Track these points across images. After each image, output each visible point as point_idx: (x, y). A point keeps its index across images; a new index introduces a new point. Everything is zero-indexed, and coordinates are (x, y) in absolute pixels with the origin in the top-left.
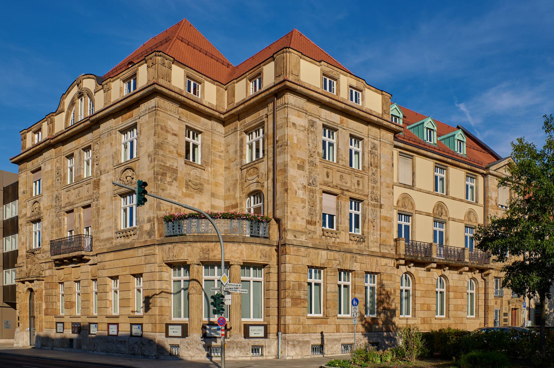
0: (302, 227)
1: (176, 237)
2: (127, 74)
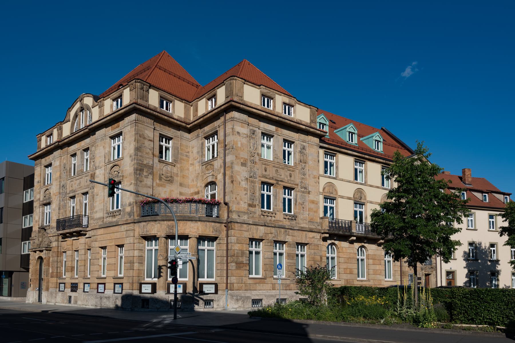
1: (149, 217)
2: (115, 95)
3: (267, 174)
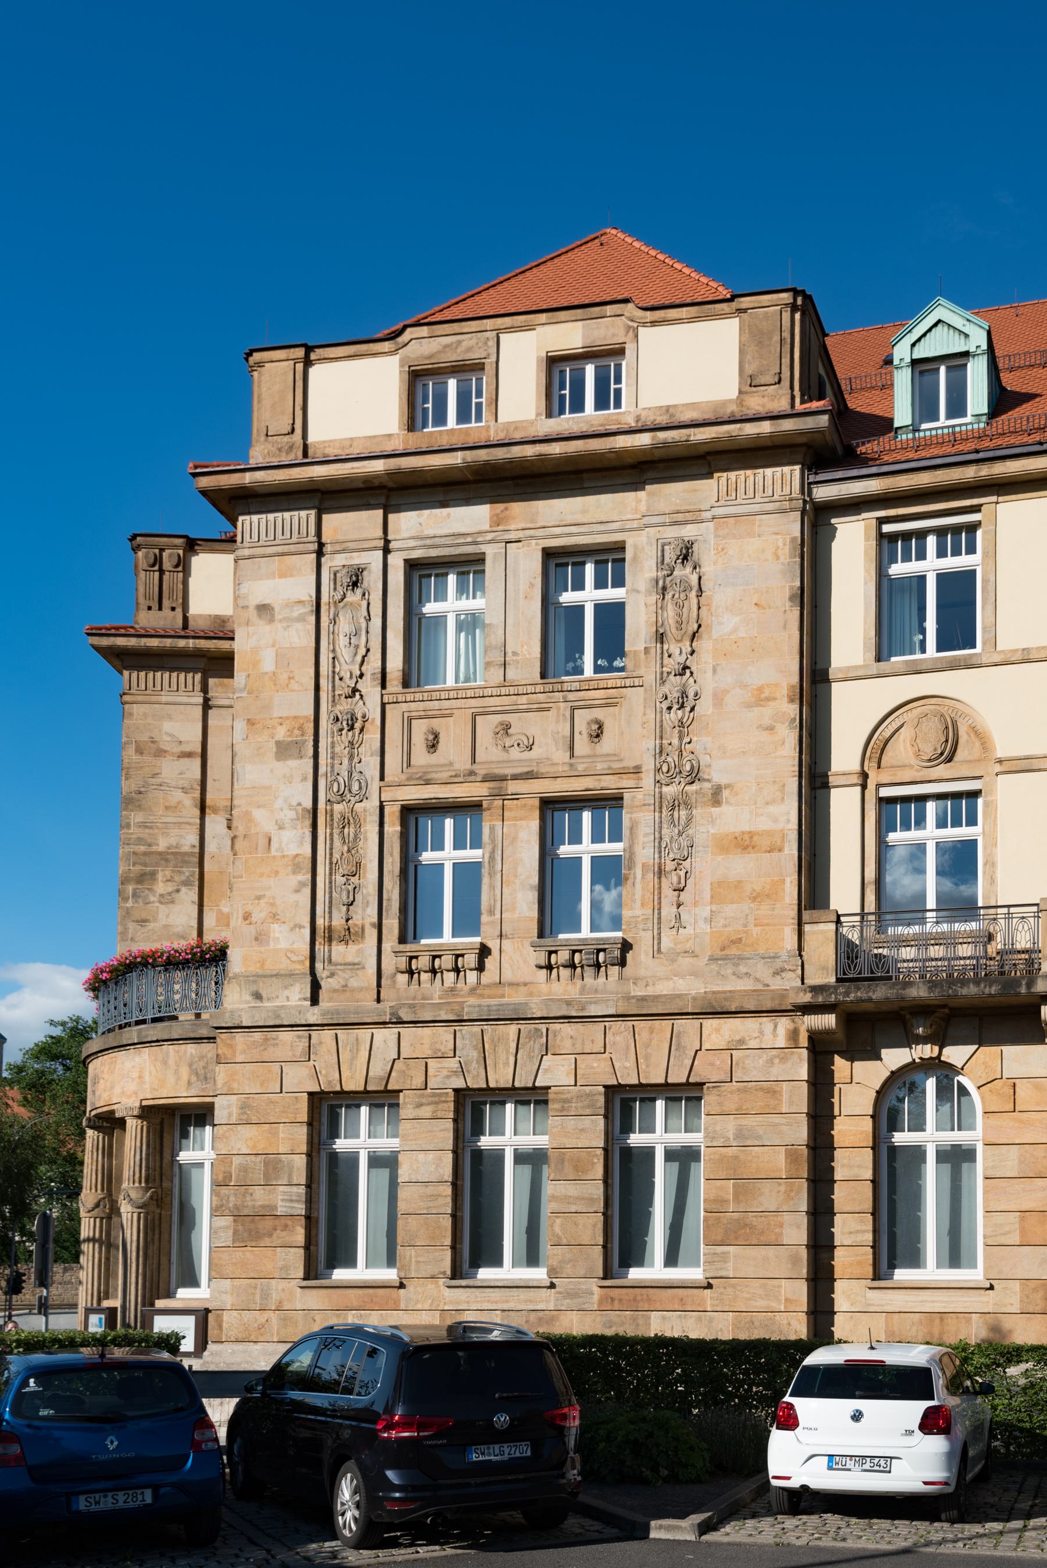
0: (294, 958)
3: (443, 761)
